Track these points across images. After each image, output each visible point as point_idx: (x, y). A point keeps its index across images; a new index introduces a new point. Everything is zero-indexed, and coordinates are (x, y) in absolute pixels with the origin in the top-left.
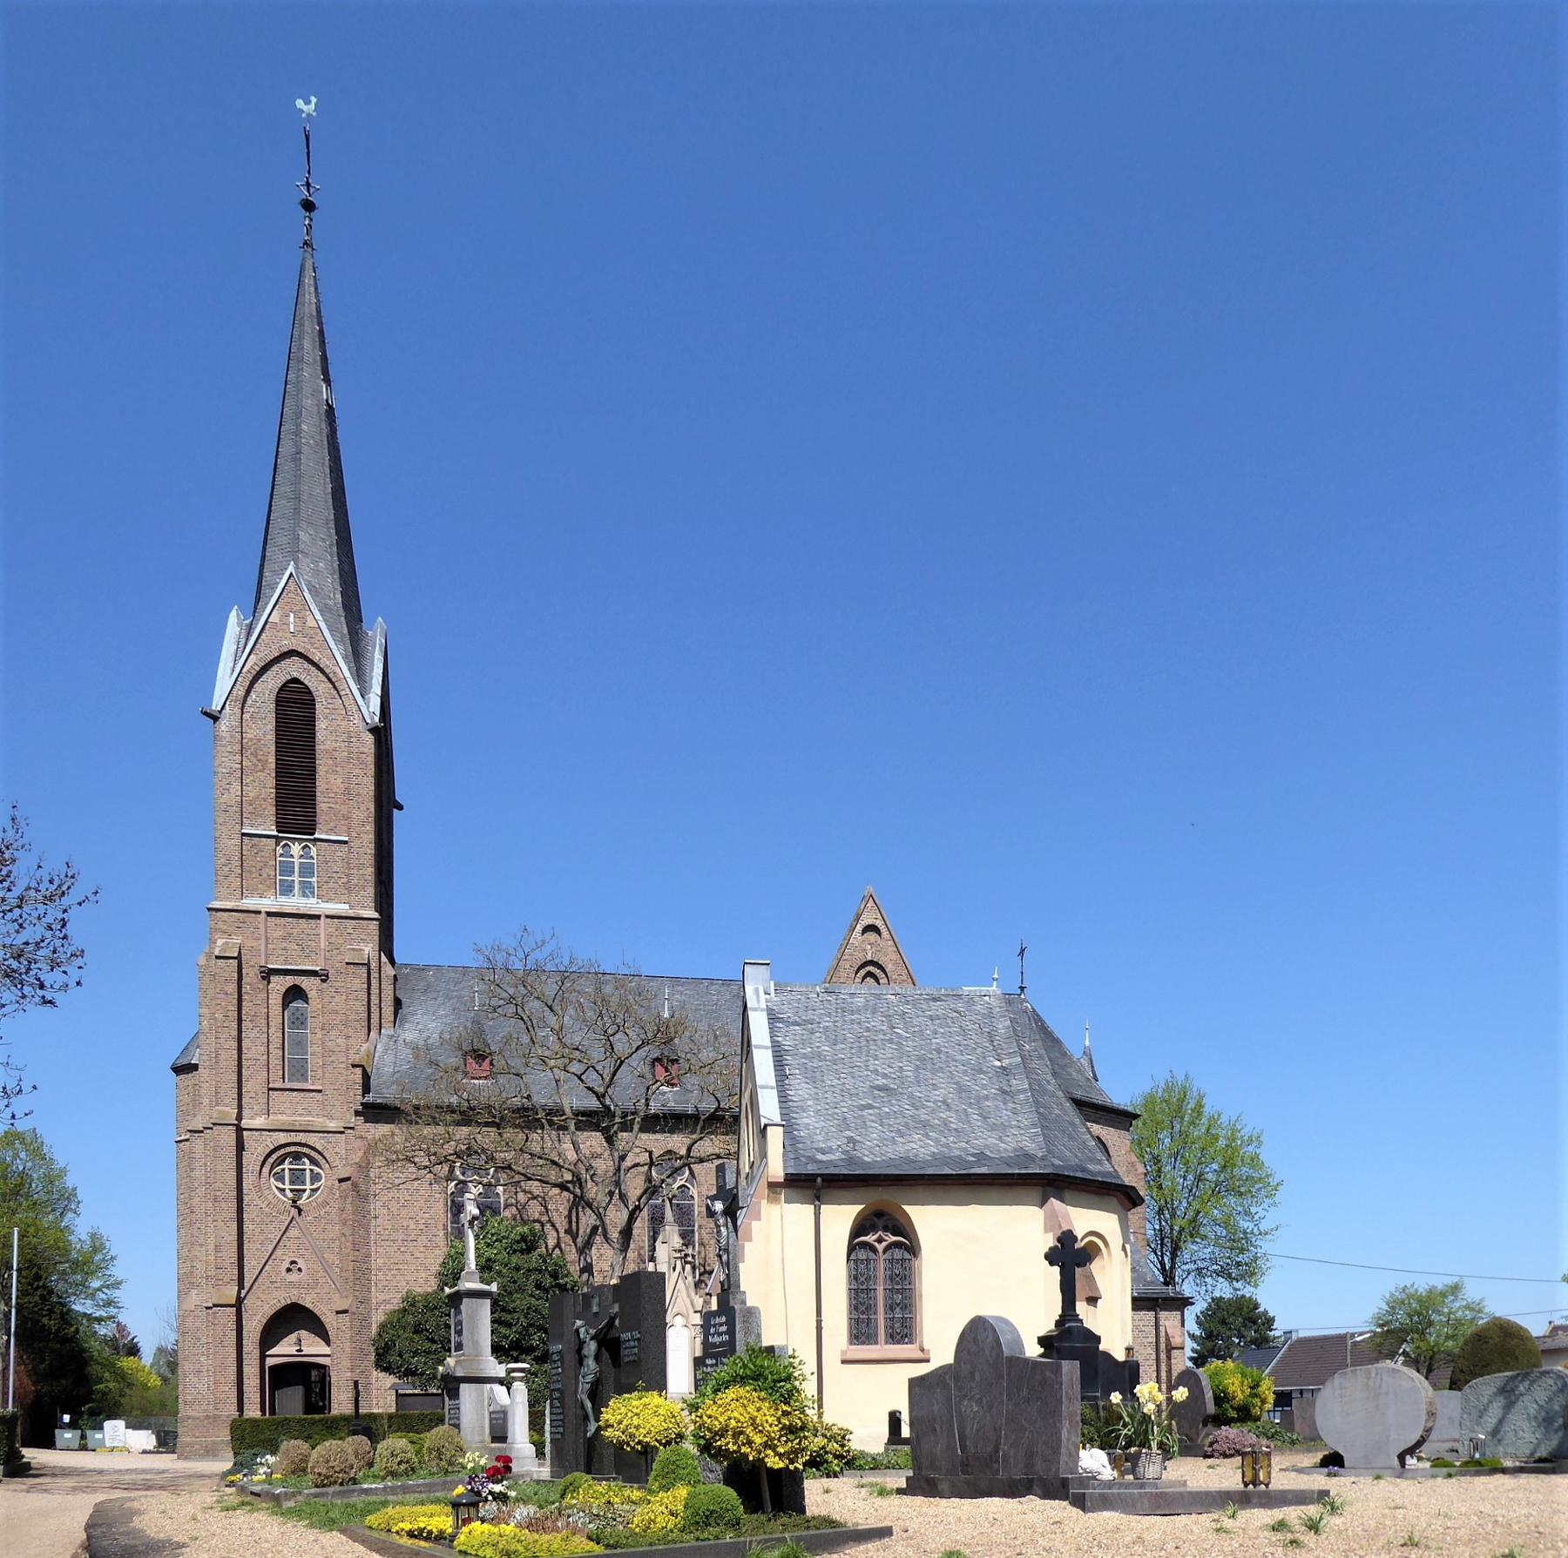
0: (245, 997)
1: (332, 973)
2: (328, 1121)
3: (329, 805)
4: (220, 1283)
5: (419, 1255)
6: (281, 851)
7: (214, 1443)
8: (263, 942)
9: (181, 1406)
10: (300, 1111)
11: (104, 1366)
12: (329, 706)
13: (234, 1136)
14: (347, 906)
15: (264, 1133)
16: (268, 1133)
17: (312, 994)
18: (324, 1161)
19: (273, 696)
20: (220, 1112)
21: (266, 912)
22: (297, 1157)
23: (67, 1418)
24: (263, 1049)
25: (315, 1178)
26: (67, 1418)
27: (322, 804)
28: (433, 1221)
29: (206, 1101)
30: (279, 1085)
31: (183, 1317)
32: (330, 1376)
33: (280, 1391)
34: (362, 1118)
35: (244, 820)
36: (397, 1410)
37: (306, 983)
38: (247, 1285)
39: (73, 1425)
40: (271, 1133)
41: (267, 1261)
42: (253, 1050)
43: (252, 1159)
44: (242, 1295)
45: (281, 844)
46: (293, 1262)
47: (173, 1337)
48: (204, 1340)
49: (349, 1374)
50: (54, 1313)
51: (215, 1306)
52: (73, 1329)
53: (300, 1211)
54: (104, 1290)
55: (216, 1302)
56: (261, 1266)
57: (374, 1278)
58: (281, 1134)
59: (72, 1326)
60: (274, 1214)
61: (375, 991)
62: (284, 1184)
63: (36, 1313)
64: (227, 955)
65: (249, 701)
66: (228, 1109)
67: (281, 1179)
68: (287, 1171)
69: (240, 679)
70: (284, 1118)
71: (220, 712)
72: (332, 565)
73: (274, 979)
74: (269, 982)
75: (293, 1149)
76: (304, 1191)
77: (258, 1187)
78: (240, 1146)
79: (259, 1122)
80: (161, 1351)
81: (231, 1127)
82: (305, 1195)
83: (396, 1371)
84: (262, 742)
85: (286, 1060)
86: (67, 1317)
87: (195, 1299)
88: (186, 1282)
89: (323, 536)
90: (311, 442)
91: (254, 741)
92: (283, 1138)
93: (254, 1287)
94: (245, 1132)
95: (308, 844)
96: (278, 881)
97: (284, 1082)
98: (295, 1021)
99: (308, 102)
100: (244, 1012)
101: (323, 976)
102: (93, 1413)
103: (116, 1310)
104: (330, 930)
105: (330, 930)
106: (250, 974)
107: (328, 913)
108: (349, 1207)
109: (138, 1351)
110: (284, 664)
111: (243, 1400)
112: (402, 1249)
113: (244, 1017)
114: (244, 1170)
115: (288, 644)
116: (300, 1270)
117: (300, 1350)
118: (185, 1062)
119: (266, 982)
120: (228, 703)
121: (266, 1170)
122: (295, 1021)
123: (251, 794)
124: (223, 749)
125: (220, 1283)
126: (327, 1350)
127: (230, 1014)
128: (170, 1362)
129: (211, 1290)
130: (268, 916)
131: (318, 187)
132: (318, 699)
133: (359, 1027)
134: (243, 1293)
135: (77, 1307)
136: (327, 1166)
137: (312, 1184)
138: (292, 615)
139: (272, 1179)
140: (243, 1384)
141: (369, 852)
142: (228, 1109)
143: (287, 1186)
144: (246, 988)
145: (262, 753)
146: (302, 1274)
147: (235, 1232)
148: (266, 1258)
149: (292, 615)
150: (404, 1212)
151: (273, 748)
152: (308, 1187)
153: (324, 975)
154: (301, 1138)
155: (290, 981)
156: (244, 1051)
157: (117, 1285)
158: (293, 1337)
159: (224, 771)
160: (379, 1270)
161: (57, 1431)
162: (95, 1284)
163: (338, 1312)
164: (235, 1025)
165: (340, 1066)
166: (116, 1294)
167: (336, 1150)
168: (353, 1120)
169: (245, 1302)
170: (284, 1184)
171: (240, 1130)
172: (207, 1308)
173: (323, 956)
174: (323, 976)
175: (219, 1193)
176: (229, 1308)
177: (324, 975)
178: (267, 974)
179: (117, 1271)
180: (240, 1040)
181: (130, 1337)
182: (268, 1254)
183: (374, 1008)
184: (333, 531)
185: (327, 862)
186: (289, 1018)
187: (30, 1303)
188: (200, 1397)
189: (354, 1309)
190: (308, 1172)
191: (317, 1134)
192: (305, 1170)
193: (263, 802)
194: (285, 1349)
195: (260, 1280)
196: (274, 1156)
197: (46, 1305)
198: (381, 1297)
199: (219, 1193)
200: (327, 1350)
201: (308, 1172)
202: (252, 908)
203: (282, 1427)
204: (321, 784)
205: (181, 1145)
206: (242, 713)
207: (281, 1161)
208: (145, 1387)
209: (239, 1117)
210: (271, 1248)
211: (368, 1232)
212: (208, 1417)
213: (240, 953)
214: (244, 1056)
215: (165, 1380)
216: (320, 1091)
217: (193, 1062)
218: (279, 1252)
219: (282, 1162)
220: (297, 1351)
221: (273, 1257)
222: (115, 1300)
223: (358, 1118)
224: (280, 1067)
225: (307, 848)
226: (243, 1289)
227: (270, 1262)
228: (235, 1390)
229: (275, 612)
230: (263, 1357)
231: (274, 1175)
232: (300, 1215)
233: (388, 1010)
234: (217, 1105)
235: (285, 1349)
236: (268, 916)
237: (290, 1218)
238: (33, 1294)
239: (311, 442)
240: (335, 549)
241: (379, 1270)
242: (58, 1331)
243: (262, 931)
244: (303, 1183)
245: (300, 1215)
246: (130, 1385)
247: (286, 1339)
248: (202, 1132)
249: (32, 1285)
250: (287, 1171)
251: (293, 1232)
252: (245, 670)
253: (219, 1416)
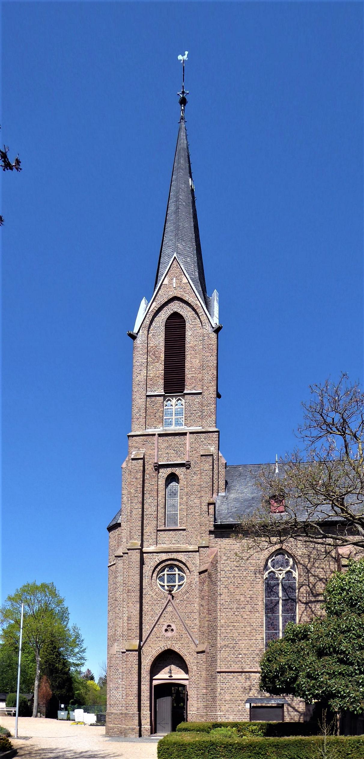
0: (146, 481)
1: (192, 463)
2: (188, 546)
3: (192, 375)
4: (130, 638)
5: (246, 617)
6: (166, 403)
7: (125, 729)
8: (156, 451)
9: (108, 706)
10: (173, 542)
11: (79, 683)
12: (193, 323)
13: (139, 555)
14: (201, 428)
15: (154, 554)
16: (156, 554)
17: (181, 477)
18: (186, 568)
19: (164, 323)
20: (132, 543)
21: (158, 434)
22: (171, 567)
23: (63, 706)
24: (155, 508)
25: (181, 578)
26: (63, 706)
27: (189, 374)
28: (255, 596)
29: (124, 540)
30: (162, 528)
31: (110, 659)
32: (187, 692)
33: (159, 699)
34: (213, 535)
35: (148, 389)
36: (250, 720)
37: (178, 471)
38: (144, 640)
39: (66, 709)
40: (158, 554)
41: (155, 625)
42: (150, 510)
43: (148, 569)
44: (141, 645)
45: (166, 400)
46: (169, 626)
47: (104, 674)
48: (120, 671)
49: (205, 691)
50: (61, 662)
51: (127, 651)
52: (68, 669)
53: (173, 597)
54: (80, 653)
55: (128, 648)
56: (152, 628)
57: (219, 631)
58: (163, 554)
59: (67, 667)
60: (159, 599)
61: (216, 472)
62: (164, 582)
63: (54, 662)
64: (137, 457)
65: (152, 328)
66: (136, 541)
67: (162, 579)
68: (166, 576)
69: (147, 316)
70: (165, 546)
71: (137, 334)
72: (194, 260)
73: (161, 470)
74: (159, 472)
75: (169, 562)
76: (175, 586)
77: (151, 585)
78: (142, 563)
79: (152, 548)
80: (101, 678)
81: (138, 551)
82: (175, 589)
83: (307, 693)
84: (158, 347)
85: (166, 515)
86: (65, 664)
87: (117, 648)
88: (112, 640)
89: (189, 246)
90: (184, 204)
91: (154, 347)
92: (164, 556)
93: (148, 640)
94: (144, 555)
95: (180, 398)
96: (164, 419)
97: (165, 527)
98: (171, 493)
99: (183, 55)
100: (145, 489)
101: (186, 466)
102: (73, 704)
103: (84, 661)
104: (191, 440)
105: (191, 440)
106: (149, 468)
107: (190, 431)
108: (206, 588)
109: (94, 678)
110: (170, 305)
111: (141, 705)
112: (236, 613)
113: (145, 492)
114: (144, 575)
115: (171, 294)
116: (172, 630)
117: (171, 676)
118: (114, 523)
119: (157, 472)
120: (141, 329)
121: (156, 573)
122: (171, 493)
123: (151, 375)
124: (138, 353)
125: (130, 638)
126: (186, 676)
127: (138, 489)
128: (104, 682)
129: (125, 642)
130: (159, 436)
131: (188, 92)
132: (187, 321)
133: (207, 490)
134: (142, 643)
135: (70, 660)
136: (188, 571)
137: (179, 582)
138: (175, 278)
139: (158, 580)
140: (141, 695)
141: (213, 396)
142: (136, 541)
143: (166, 584)
144: (147, 476)
145: (157, 353)
146: (174, 632)
147: (138, 609)
148: (154, 624)
149: (175, 278)
150: (237, 591)
151: (163, 349)
152: (177, 583)
153: (189, 465)
154: (174, 556)
155: (169, 471)
156: (145, 510)
157: (83, 651)
158: (167, 669)
159: (138, 364)
160: (222, 626)
161: (59, 712)
162: (76, 650)
163: (198, 653)
164: (140, 495)
165: (196, 515)
166: (84, 655)
167: (194, 561)
168: (207, 539)
169: (143, 649)
170: (164, 582)
171: (142, 553)
172: (123, 652)
173: (187, 455)
174: (186, 466)
175: (130, 588)
176: (134, 652)
177: (189, 465)
178: (158, 467)
179: (84, 645)
180: (143, 504)
181: (91, 674)
182: (155, 622)
183: (215, 480)
184: (194, 244)
185: (190, 405)
186: (168, 492)
187: (52, 658)
188: (118, 702)
189: (208, 651)
190: (177, 576)
191: (183, 553)
192: (175, 574)
193: (157, 378)
194: (163, 676)
195: (151, 636)
196: (159, 567)
197: (58, 659)
198: (223, 643)
199: (130, 588)
200: (186, 676)
201: (177, 576)
202: (152, 433)
203: (209, 752)
204: (187, 365)
205: (111, 568)
206: (148, 334)
207: (163, 570)
208: (95, 690)
209: (142, 545)
210: (157, 618)
211: (216, 603)
212: (122, 714)
213: (144, 456)
214: (145, 513)
215: (101, 688)
216: (184, 530)
217: (118, 522)
218: (161, 620)
219: (163, 570)
220: (169, 677)
221: (158, 623)
222: (84, 657)
223: (211, 535)
224: (163, 518)
225: (180, 401)
226: (142, 641)
227: (157, 626)
228: (136, 699)
229: (166, 278)
230: (151, 680)
231: (159, 578)
232: (173, 599)
233: (222, 483)
234: (131, 539)
235: (163, 676)
236: (159, 436)
237: (168, 601)
238: (53, 655)
239: (184, 204)
240: (195, 252)
241: (222, 626)
242: (62, 669)
243: (156, 445)
244: (175, 582)
245: (173, 599)
246: (89, 691)
247: (163, 670)
248: (122, 556)
249: (52, 651)
250: (166, 576)
251: (169, 609)
252: (150, 311)
253: (128, 714)
